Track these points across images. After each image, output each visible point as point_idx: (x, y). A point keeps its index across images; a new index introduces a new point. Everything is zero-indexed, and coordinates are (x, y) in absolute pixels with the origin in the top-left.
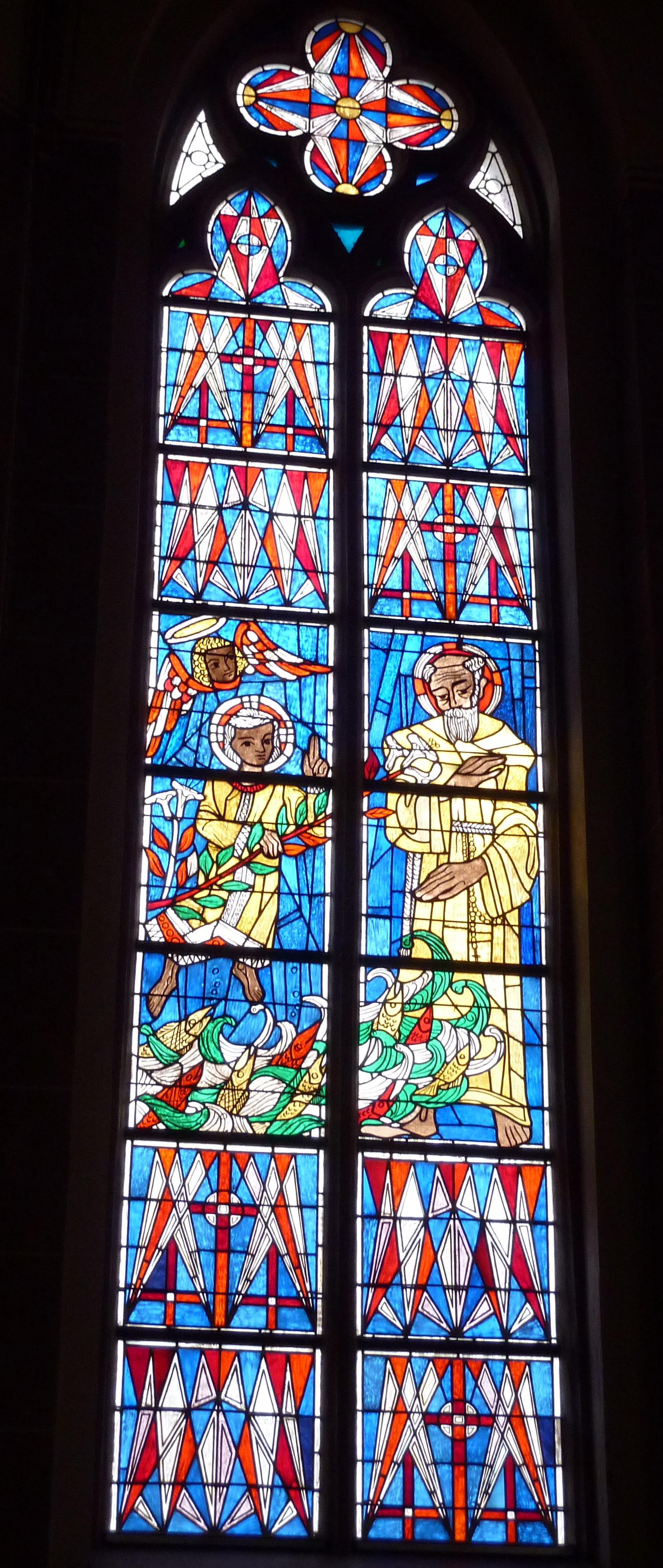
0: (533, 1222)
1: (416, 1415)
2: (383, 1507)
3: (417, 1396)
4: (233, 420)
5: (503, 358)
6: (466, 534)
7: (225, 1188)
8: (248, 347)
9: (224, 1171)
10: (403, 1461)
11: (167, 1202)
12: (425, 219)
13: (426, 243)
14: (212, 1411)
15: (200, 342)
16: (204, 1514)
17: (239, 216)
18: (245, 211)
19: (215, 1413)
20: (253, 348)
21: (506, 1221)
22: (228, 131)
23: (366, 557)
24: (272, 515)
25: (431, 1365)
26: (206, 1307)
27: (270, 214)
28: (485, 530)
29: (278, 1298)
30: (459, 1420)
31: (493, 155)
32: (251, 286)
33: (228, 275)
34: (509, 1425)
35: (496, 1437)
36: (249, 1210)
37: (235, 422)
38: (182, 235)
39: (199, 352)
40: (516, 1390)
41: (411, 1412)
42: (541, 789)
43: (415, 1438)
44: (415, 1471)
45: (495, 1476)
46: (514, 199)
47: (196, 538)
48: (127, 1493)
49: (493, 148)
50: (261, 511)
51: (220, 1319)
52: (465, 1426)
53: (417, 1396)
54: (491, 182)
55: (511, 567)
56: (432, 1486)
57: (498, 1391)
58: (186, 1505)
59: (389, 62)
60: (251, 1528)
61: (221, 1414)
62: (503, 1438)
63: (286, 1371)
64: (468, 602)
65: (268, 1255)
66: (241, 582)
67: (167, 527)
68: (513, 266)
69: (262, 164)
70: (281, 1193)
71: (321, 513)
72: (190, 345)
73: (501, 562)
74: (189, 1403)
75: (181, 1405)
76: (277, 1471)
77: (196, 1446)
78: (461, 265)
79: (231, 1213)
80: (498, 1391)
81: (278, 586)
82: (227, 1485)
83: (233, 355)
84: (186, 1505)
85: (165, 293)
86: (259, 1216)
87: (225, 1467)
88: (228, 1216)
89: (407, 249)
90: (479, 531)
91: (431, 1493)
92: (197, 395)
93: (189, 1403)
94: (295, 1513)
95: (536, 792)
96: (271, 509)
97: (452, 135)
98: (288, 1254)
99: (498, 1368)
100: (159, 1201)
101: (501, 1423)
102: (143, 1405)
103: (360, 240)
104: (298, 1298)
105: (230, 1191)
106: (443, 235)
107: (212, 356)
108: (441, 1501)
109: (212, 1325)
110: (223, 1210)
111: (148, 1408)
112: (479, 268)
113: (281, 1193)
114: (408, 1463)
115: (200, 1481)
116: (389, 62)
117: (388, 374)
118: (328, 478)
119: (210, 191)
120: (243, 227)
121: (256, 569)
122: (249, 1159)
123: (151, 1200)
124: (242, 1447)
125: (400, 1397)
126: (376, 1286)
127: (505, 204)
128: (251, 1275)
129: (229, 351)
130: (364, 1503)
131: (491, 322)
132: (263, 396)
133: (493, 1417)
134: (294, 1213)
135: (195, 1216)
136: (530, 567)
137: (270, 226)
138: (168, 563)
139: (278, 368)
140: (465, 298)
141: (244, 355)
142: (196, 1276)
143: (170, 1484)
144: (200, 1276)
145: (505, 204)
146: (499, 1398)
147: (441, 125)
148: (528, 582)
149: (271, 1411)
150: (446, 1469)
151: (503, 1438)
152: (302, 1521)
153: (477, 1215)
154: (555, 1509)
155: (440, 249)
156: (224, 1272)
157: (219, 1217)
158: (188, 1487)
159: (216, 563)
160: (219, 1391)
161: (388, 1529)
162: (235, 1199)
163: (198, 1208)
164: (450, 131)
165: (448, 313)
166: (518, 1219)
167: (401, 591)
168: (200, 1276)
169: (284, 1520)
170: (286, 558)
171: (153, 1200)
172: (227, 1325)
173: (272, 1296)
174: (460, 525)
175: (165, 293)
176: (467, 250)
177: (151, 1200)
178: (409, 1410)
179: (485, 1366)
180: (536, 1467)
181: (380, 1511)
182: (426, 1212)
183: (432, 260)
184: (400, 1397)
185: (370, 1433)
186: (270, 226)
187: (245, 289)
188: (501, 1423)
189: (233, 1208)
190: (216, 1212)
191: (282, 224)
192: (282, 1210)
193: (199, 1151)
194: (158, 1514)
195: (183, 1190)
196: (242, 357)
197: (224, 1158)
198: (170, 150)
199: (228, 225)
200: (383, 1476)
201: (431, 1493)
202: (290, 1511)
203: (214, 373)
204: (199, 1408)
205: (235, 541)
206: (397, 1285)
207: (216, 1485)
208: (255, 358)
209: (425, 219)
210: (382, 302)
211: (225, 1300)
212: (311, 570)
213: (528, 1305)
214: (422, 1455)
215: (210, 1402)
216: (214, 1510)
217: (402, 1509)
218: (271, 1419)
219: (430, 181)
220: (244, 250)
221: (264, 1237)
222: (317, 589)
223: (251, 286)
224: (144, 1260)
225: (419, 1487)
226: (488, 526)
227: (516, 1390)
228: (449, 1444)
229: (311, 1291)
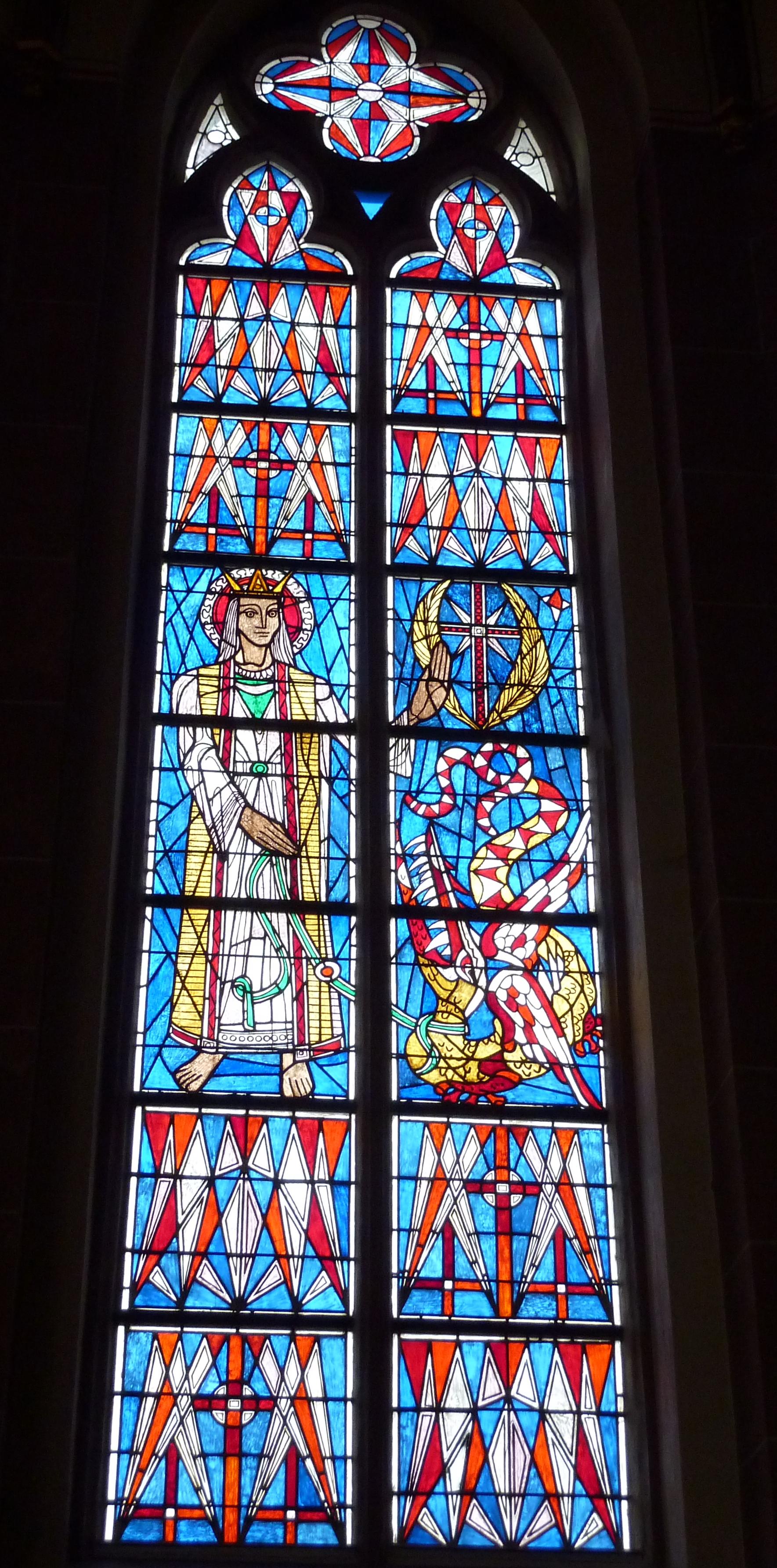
0: (333, 1183)
2: (139, 1506)
3: (187, 1378)
4: (461, 391)
5: (208, 293)
6: (281, 470)
7: (501, 1165)
8: (474, 323)
10: (166, 1454)
11: (439, 1181)
12: (246, 173)
13: (247, 197)
14: (501, 1410)
15: (424, 318)
17: (463, 204)
18: (470, 200)
20: (479, 324)
21: (305, 1181)
22: (245, 109)
23: (170, 493)
24: (505, 480)
26: (489, 1294)
27: (495, 200)
29: (568, 1285)
30: (234, 1404)
31: (523, 130)
32: (479, 268)
33: (457, 258)
38: (196, 208)
39: (425, 328)
41: (179, 1394)
42: (582, 734)
43: (181, 1428)
46: (547, 170)
47: (429, 504)
49: (522, 124)
51: (506, 1308)
52: (241, 1411)
53: (187, 1378)
54: (527, 157)
55: (330, 503)
56: (200, 1483)
57: (282, 1370)
58: (476, 1518)
59: (414, 48)
60: (552, 1541)
61: (512, 1413)
62: (285, 1424)
64: (280, 537)
65: (554, 1238)
66: (476, 547)
68: (548, 229)
69: (282, 138)
74: (475, 1403)
75: (466, 1405)
76: (578, 1477)
78: (284, 214)
80: (282, 1370)
81: (516, 550)
84: (476, 1518)
86: (542, 1195)
87: (519, 1474)
88: (508, 1196)
89: (226, 201)
91: (197, 1490)
92: (424, 368)
93: (475, 1403)
94: (601, 1525)
95: (576, 736)
96: (503, 475)
97: (480, 113)
98: (576, 1237)
100: (432, 1181)
102: (423, 1405)
103: (381, 210)
104: (590, 1284)
106: (264, 188)
108: (209, 1498)
109: (497, 1315)
110: (503, 1188)
112: (305, 216)
114: (172, 1456)
115: (491, 1491)
116: (414, 48)
117: (204, 317)
119: (225, 164)
120: (468, 213)
121: (493, 533)
122: (527, 1134)
123: (421, 1179)
125: (167, 1379)
126: (148, 1252)
127: (539, 173)
128: (538, 1260)
130: (117, 1502)
131: (315, 266)
132: (491, 369)
133: (273, 1400)
136: (350, 502)
137: (495, 212)
140: (287, 246)
142: (476, 1262)
143: (457, 1494)
145: (539, 173)
146: (283, 1379)
147: (467, 104)
149: (567, 1408)
150: (215, 1463)
151: (285, 1424)
152: (609, 1533)
153: (271, 1175)
155: (261, 200)
158: (479, 1497)
159: (449, 529)
160: (508, 1387)
161: (144, 1533)
164: (477, 110)
165: (270, 258)
166: (316, 1178)
167: (303, 532)
169: (588, 1532)
171: (425, 1179)
174: (275, 461)
175: (393, 274)
176: (292, 201)
177: (421, 1179)
178: (176, 1391)
180: (323, 1459)
181: (134, 1511)
182: (213, 1170)
183: (253, 211)
184: (167, 1379)
186: (495, 212)
190: (494, 1191)
191: (507, 210)
192: (566, 1188)
193: (472, 1126)
194: (445, 1529)
197: (501, 1132)
198: (187, 129)
199: (452, 211)
200: (141, 1471)
201: (197, 1490)
203: (442, 350)
206: (172, 1252)
207: (241, 1256)
208: (482, 333)
209: (246, 173)
210: (199, 252)
211: (509, 1287)
213: (324, 1273)
214: (188, 1445)
215: (498, 1401)
216: (510, 1524)
219: (457, 152)
220: (470, 233)
221: (549, 1216)
223: (479, 268)
224: (418, 1245)
225: (183, 1481)
228: (221, 1430)
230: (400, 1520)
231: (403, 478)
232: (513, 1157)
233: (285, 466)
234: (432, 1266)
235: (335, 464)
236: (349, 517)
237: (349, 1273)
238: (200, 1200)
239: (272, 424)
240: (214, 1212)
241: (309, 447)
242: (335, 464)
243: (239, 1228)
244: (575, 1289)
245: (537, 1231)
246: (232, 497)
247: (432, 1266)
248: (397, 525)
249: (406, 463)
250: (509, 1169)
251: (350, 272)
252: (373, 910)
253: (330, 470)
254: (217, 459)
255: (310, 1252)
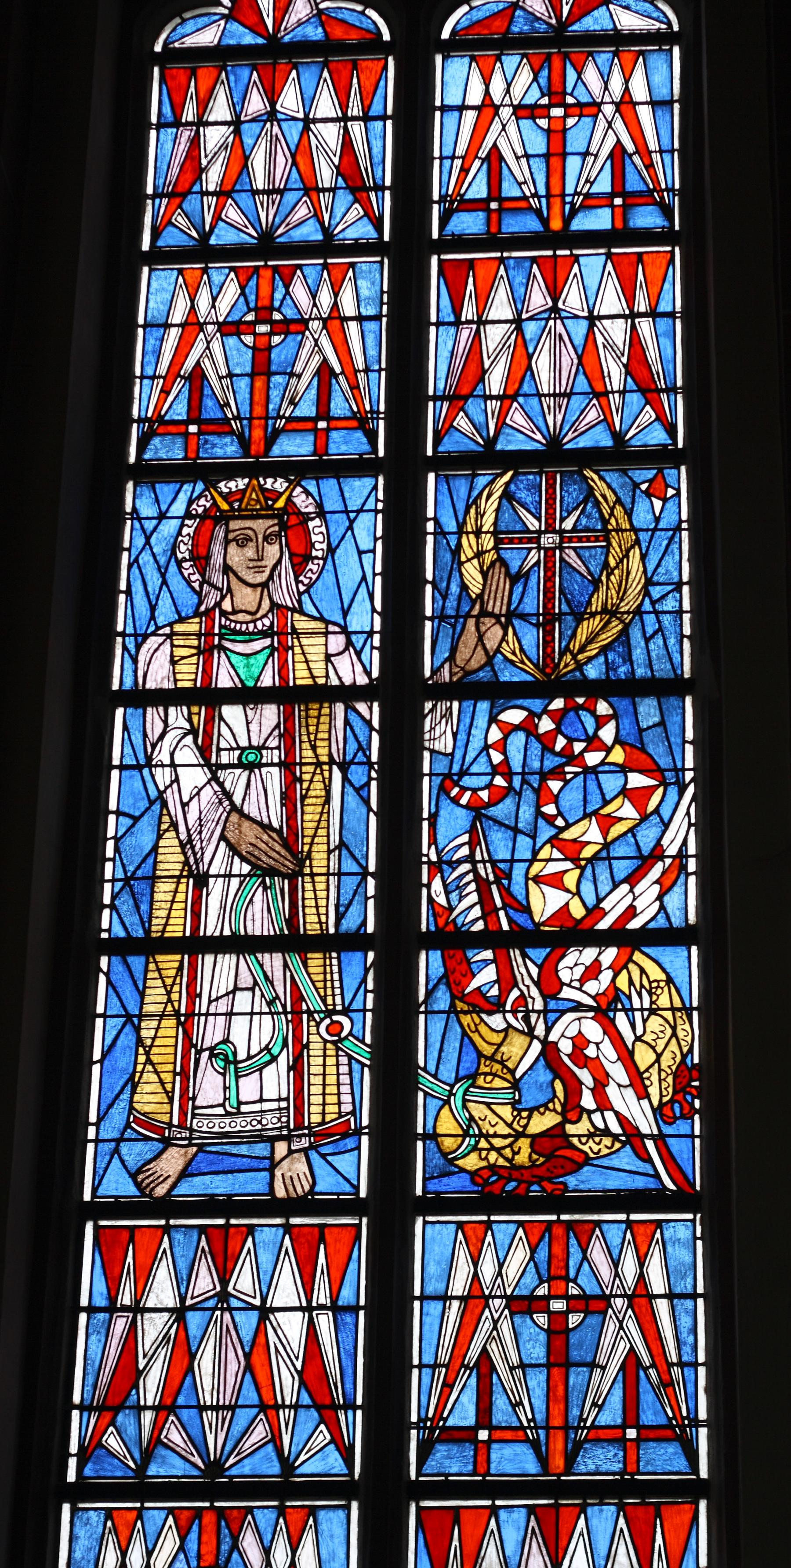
1: (497, 1302)
4: (535, 195)
9: (557, 1250)
15: (487, 93)
16: (202, 1449)
19: (218, 1313)
20: (564, 93)
24: (592, 319)
25: (521, 1232)
28: (608, 110)
34: (630, 1312)
35: (611, 1327)
36: (595, 1304)
37: (539, 197)
40: (641, 1261)
44: (495, 1377)
45: (607, 1380)
48: (93, 1422)
50: (576, 317)
51: (558, 1462)
63: (655, 1532)
65: (623, 1368)
67: (444, 354)
70: (641, 1279)
71: (376, 109)
72: (475, 97)
73: (630, 147)
77: (192, 1356)
79: (569, 1310)
82: (232, 1408)
83: (535, 106)
85: (445, 34)
86: (610, 1311)
90: (600, 110)
99: (614, 1234)
101: (619, 1305)
105: (567, 1279)
107: (506, 113)
108: (530, 1416)
110: (558, 1305)
111: (124, 1308)
113: (641, 1279)
115: (194, 1403)
118: (672, 261)
121: (574, 398)
124: (256, 1357)
128: (602, 1396)
129: (529, 100)
133: (605, 1300)
134: (662, 1307)
135: (517, 1319)
138: (165, 201)
139: (601, 116)
141: (551, 105)
144: (526, 1402)
148: (669, 173)
154: (696, 1423)
156: (558, 1394)
157: (551, 1315)
162: (573, 1291)
163: (522, 1305)
168: (526, 1402)
170: (326, 175)
171: (456, 1298)
172: (569, 1468)
173: (631, 1427)
175: (445, 34)
179: (598, 1232)
185: (431, 1332)
187: (559, 17)
188: (619, 1305)
189: (572, 1302)
192: (643, 1301)
193: (520, 1224)
195: (499, 1280)
196: (548, 107)
197: (558, 1231)
202: (321, 1437)
204: (193, 1308)
205: (542, 364)
207: (216, 1408)
212: (648, 389)
217: (474, 1429)
218: (278, 1302)
221: (617, 1339)
222: (660, 417)
226: (613, 102)
227: (641, 1261)
229: (688, 1417)
230: (436, 422)
231: (452, 330)
232: (573, 1263)
233: (293, 327)
234: (463, 1412)
235: (360, 319)
236: (377, 391)
237: (355, 1426)
238: (224, 146)
239: (275, 269)
240: (183, 1354)
241: (325, 298)
242: (360, 319)
243: (214, 1371)
244: (649, 1434)
245: (601, 1359)
246: (221, 378)
247: (463, 1412)
248: (442, 398)
249: (457, 309)
250: (567, 1279)
251: (387, 37)
252: (395, 942)
253: (353, 328)
254: (201, 327)
255: (306, 1399)
